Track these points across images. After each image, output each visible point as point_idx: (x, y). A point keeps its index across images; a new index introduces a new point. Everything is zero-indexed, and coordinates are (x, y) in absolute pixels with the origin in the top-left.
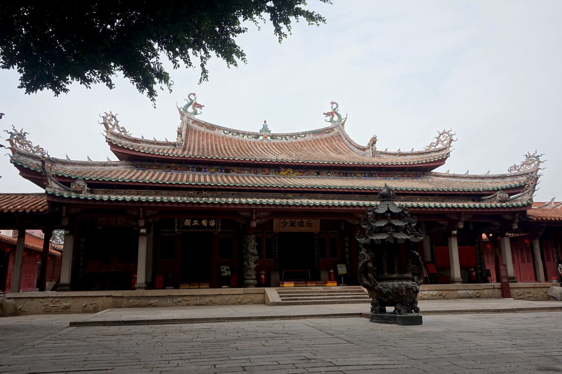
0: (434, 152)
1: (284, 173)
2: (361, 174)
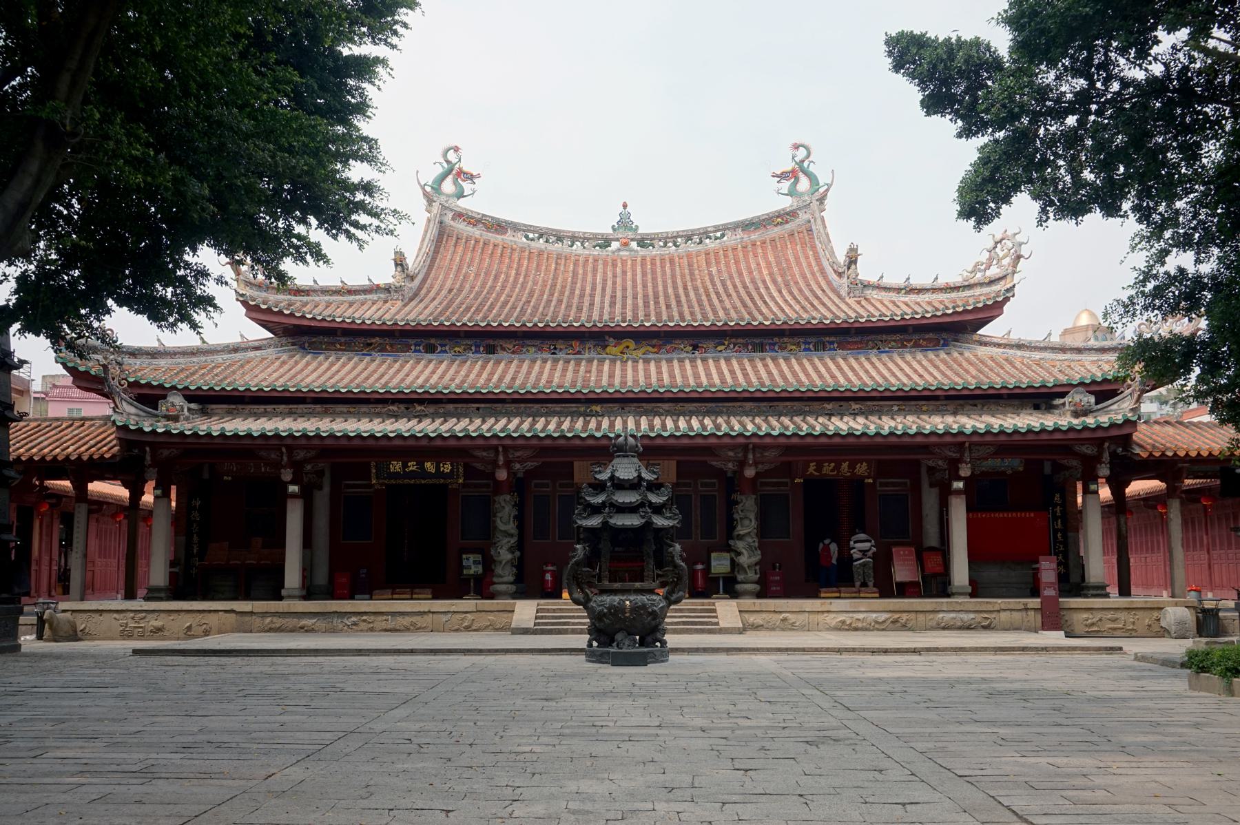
0: (981, 284)
1: (616, 350)
2: (798, 345)
